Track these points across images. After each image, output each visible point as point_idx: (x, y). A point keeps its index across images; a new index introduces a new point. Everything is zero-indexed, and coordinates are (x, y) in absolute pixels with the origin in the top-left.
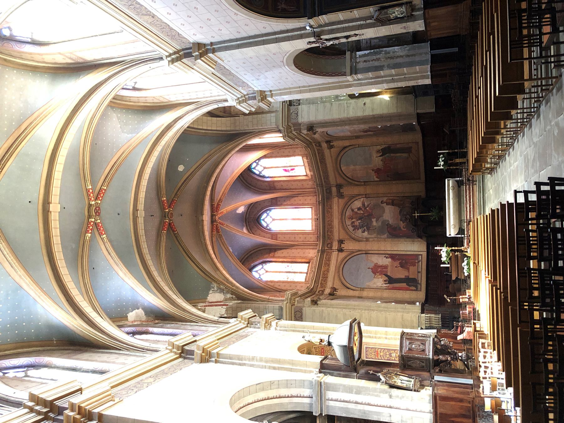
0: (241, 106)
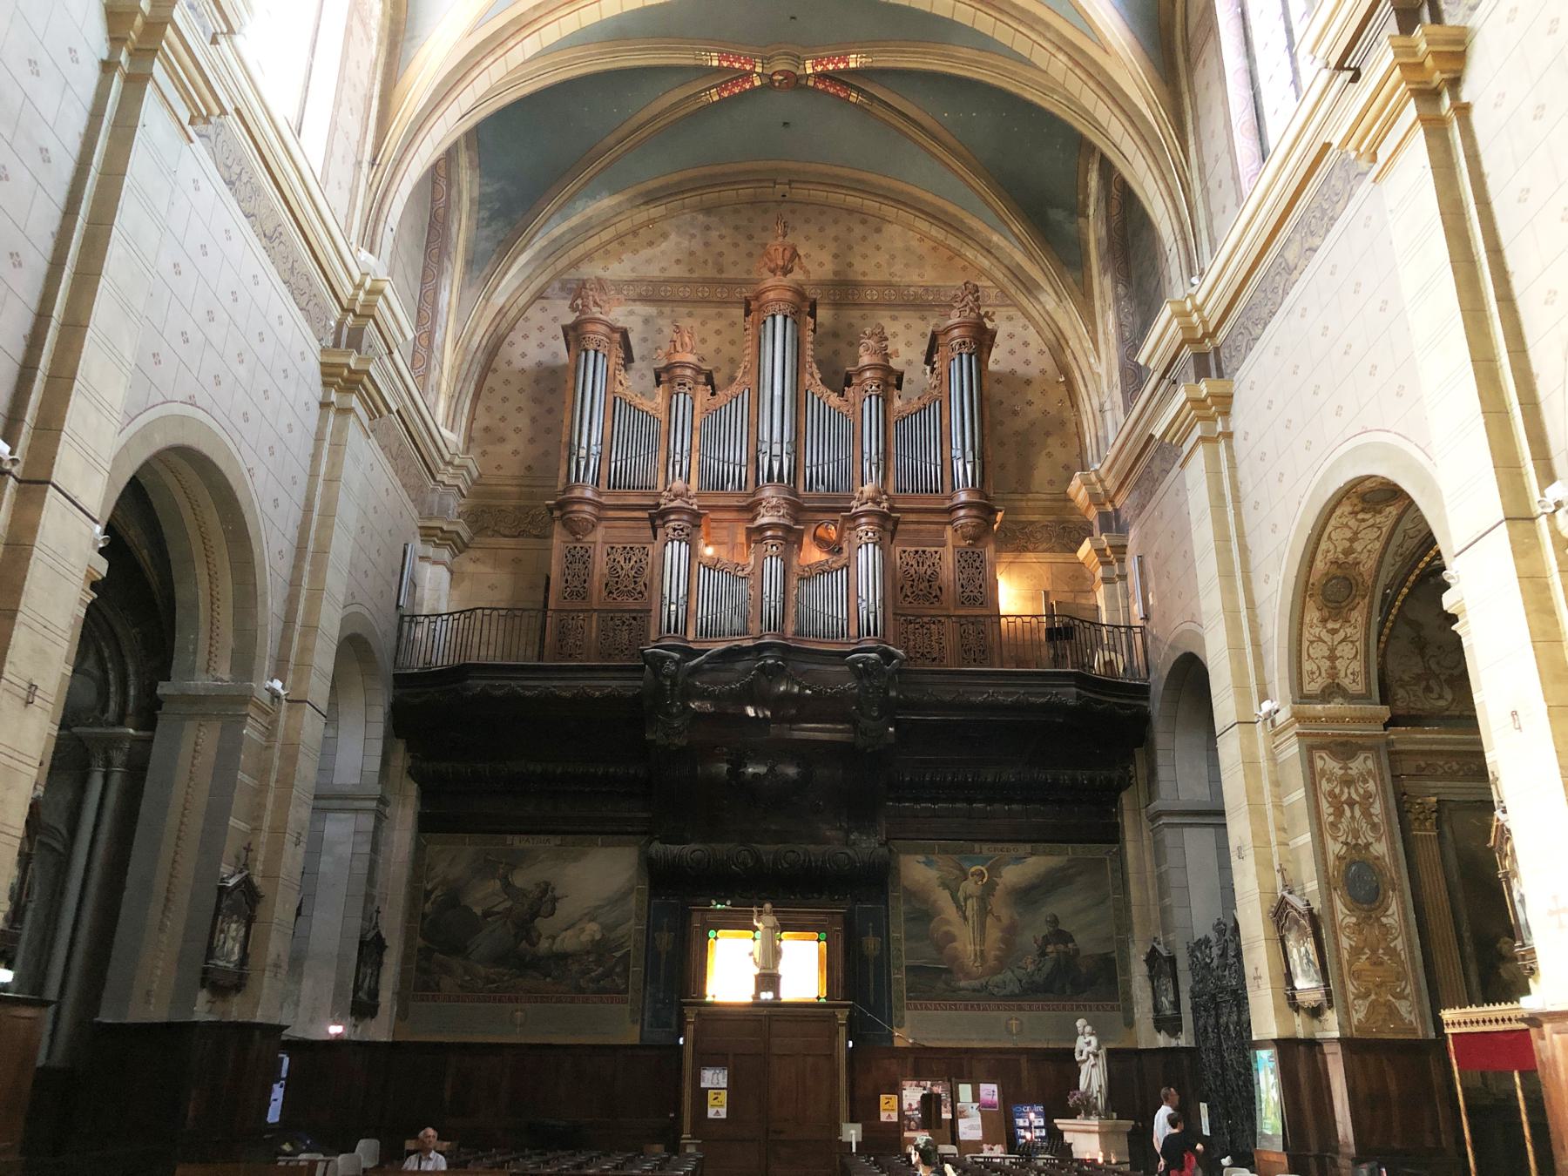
0: (1169, 322)
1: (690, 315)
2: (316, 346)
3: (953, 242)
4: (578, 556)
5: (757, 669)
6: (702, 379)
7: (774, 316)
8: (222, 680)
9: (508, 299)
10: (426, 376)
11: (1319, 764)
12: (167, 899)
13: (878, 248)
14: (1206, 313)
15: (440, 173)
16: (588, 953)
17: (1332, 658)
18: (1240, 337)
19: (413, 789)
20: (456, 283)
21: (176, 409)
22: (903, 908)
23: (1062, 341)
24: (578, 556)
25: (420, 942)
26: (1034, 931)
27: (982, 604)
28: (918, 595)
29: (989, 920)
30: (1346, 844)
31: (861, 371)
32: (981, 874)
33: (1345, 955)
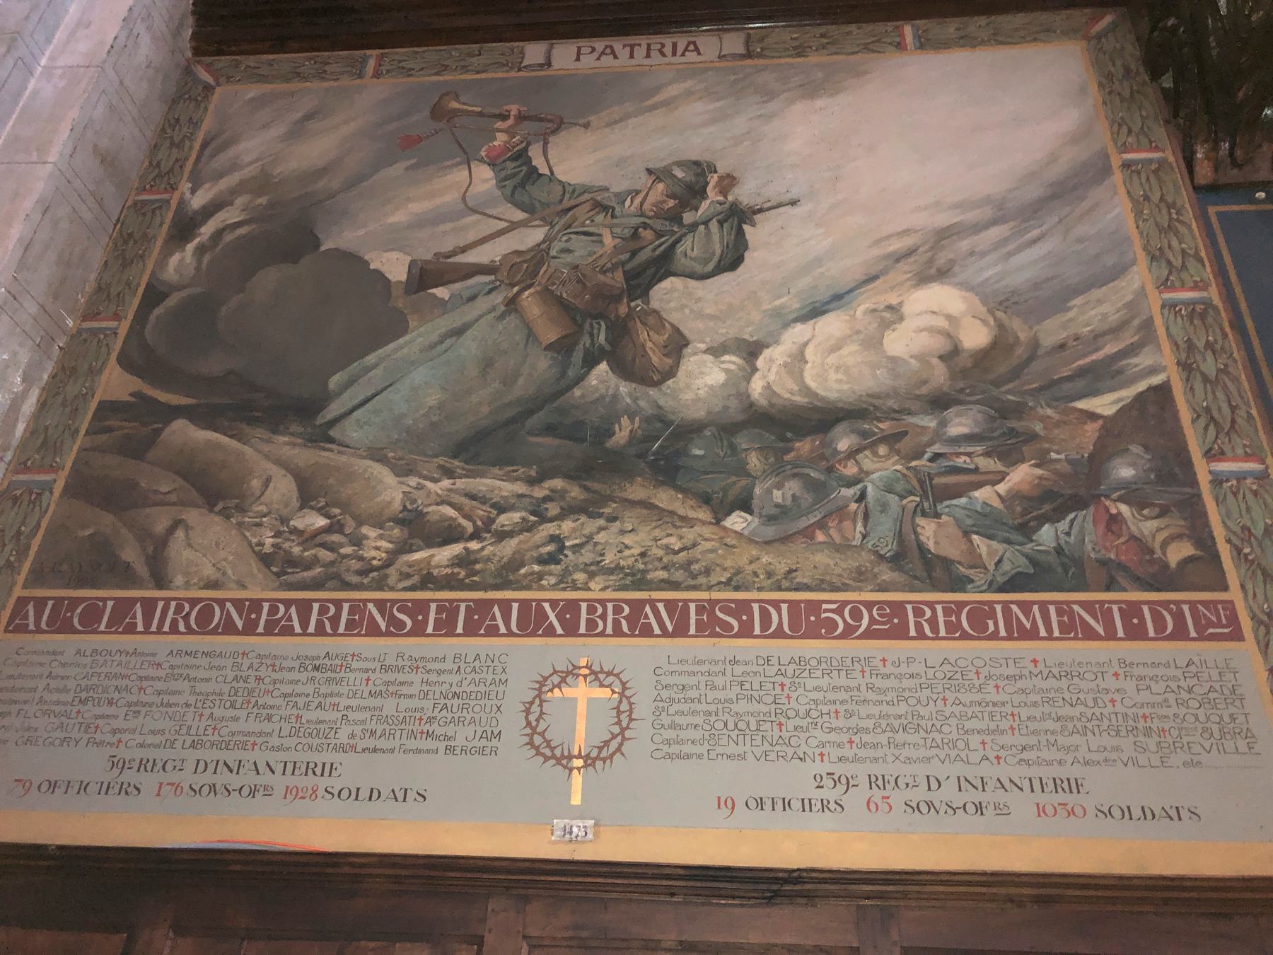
16: (940, 403)
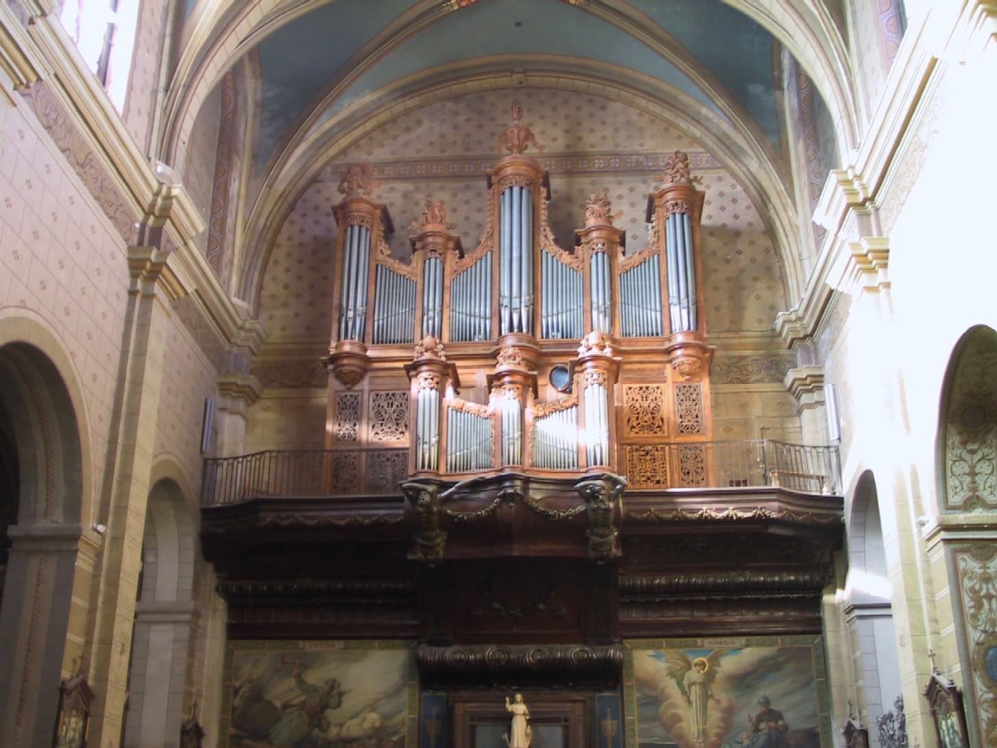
1: (442, 188)
2: (123, 246)
3: (668, 115)
4: (348, 403)
5: (500, 497)
6: (451, 245)
7: (511, 188)
8: (57, 522)
9: (289, 184)
10: (220, 256)
11: (962, 565)
12: (22, 699)
13: (604, 123)
14: (864, 181)
15: (227, 87)
16: (370, 738)
17: (973, 474)
18: (892, 201)
19: (221, 604)
20: (244, 175)
21: (10, 313)
22: (636, 695)
23: (764, 197)
24: (348, 403)
25: (232, 731)
26: (750, 710)
27: (698, 431)
28: (643, 426)
29: (711, 703)
30: (985, 631)
31: (587, 233)
32: (703, 664)
33: (984, 726)
